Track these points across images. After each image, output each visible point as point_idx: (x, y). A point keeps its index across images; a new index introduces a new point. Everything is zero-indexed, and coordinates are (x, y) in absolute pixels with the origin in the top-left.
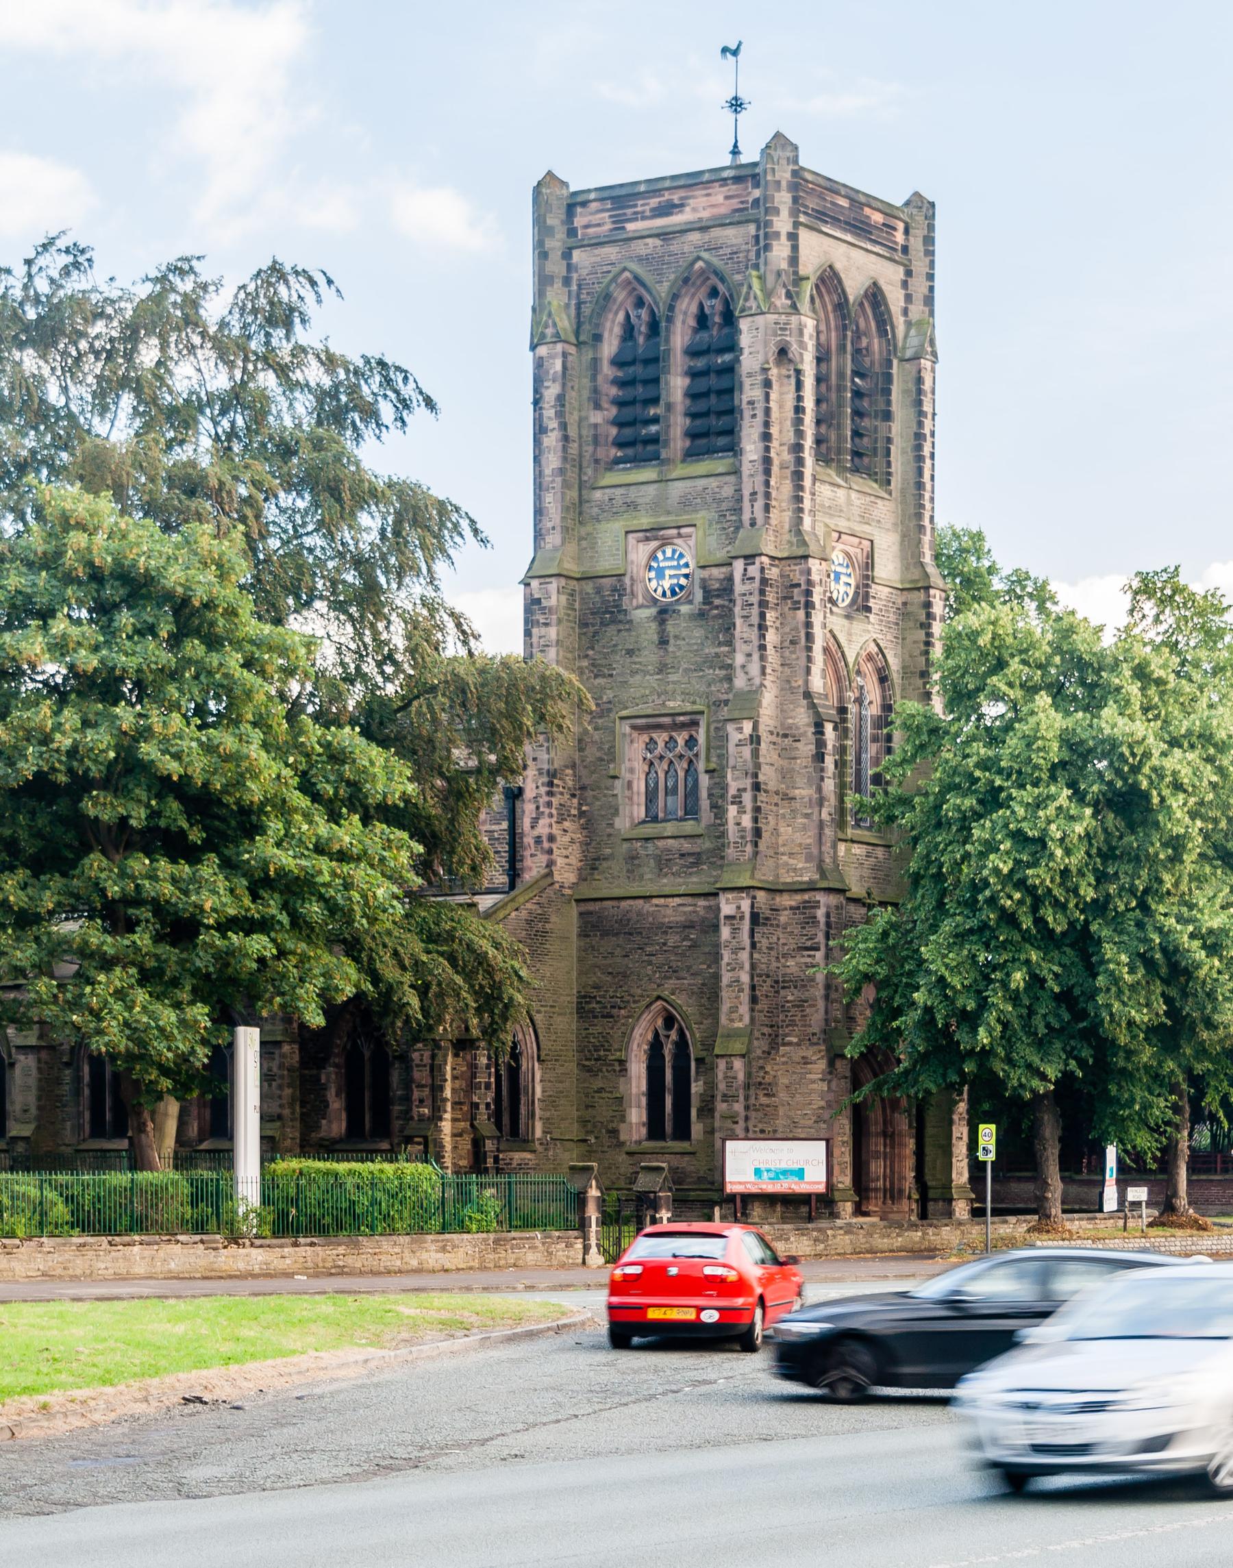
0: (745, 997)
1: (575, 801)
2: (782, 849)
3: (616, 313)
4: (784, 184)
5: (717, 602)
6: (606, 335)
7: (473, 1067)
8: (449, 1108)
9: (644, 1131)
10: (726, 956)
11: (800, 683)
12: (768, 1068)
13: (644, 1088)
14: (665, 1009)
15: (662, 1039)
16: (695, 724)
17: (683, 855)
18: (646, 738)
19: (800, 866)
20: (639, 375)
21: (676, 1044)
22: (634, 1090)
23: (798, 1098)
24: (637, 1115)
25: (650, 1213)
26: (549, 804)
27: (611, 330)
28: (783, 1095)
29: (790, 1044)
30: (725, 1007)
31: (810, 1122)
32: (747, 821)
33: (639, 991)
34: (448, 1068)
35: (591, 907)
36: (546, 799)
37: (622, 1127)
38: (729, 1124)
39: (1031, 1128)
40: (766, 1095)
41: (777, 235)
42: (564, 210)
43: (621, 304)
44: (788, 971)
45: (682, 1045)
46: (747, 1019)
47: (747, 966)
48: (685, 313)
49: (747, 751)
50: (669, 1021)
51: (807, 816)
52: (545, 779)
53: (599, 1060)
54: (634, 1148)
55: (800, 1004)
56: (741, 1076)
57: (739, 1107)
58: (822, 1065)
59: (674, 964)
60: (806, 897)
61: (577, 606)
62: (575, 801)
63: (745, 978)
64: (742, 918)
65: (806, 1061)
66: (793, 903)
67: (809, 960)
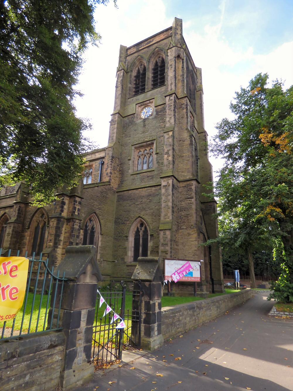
0: (170, 210)
1: (119, 167)
2: (179, 171)
3: (136, 68)
4: (179, 25)
5: (159, 114)
6: (133, 72)
7: (73, 229)
8: (62, 244)
9: (132, 259)
10: (163, 198)
11: (185, 127)
12: (177, 236)
13: (133, 245)
14: (141, 221)
15: (140, 230)
16: (153, 144)
17: (148, 177)
18: (138, 151)
19: (186, 174)
20: (141, 77)
21: (144, 231)
22: (130, 246)
23: (187, 247)
24: (130, 253)
25: (145, 299)
26: (111, 164)
27: (135, 71)
28: (181, 246)
29: (183, 229)
30: (163, 214)
31: (191, 256)
32: (170, 158)
33: (133, 216)
34: (64, 229)
35: (121, 193)
36: (110, 163)
37: (126, 257)
38: (164, 254)
39: (135, 280)
40: (176, 245)
41: (178, 33)
42: (126, 50)
43: (137, 66)
44: (182, 206)
45: (146, 231)
46: (171, 218)
47: (171, 200)
48: (153, 62)
49: (171, 140)
50: (142, 224)
51: (188, 160)
52: (111, 158)
53: (120, 237)
54: (129, 264)
55: (187, 216)
56: (169, 237)
57: (168, 248)
58: (195, 235)
59: (144, 207)
60: (188, 183)
61: (122, 123)
62: (119, 167)
63: (170, 204)
64: (169, 186)
65: (189, 234)
66: (184, 185)
67: (189, 202)
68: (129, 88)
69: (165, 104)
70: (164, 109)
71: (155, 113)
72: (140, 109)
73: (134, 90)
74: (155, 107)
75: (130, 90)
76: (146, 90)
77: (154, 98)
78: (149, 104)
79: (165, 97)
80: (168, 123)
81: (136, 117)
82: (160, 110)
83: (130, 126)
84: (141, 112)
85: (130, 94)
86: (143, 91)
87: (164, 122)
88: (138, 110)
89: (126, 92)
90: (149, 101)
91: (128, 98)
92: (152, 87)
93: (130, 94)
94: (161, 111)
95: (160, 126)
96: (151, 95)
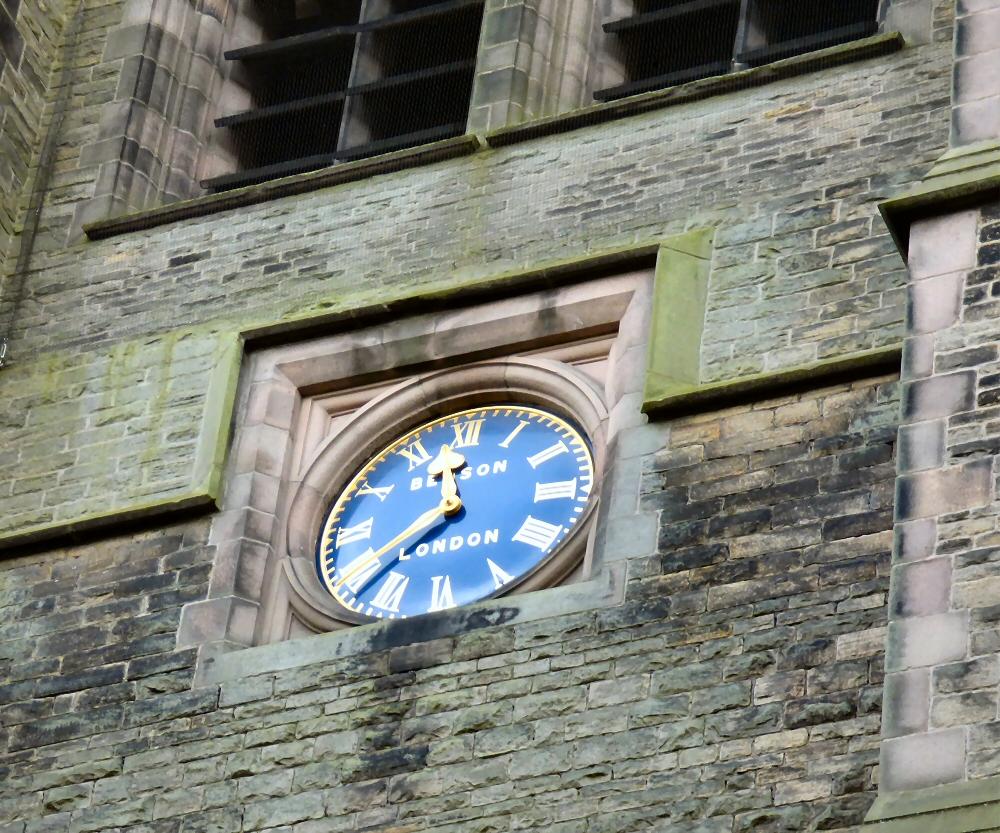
5: (744, 546)
68: (134, 49)
69: (888, 365)
70: (870, 464)
71: (637, 534)
72: (323, 437)
73: (234, 102)
74: (662, 413)
75: (145, 86)
76: (486, 116)
77: (642, 262)
78: (539, 368)
79: (903, 219)
80: (949, 709)
81: (220, 569)
82: (758, 476)
83: (63, 735)
84: (334, 502)
85: (132, 152)
86: (426, 108)
87: (860, 700)
88: (275, 444)
89: (62, 110)
90: (524, 308)
91: (96, 215)
92: (612, 76)
93: (132, 152)
94: (768, 507)
95: (734, 777)
96: (580, 209)
